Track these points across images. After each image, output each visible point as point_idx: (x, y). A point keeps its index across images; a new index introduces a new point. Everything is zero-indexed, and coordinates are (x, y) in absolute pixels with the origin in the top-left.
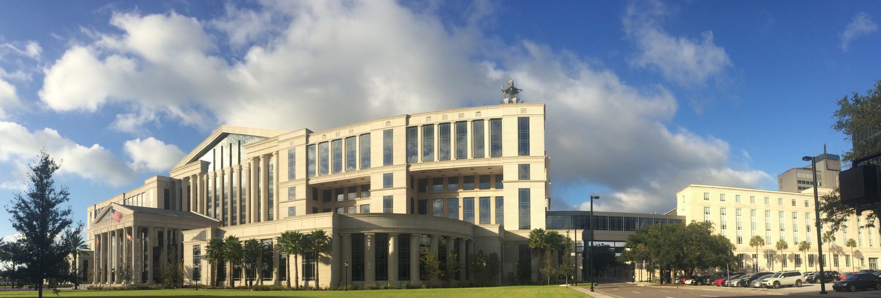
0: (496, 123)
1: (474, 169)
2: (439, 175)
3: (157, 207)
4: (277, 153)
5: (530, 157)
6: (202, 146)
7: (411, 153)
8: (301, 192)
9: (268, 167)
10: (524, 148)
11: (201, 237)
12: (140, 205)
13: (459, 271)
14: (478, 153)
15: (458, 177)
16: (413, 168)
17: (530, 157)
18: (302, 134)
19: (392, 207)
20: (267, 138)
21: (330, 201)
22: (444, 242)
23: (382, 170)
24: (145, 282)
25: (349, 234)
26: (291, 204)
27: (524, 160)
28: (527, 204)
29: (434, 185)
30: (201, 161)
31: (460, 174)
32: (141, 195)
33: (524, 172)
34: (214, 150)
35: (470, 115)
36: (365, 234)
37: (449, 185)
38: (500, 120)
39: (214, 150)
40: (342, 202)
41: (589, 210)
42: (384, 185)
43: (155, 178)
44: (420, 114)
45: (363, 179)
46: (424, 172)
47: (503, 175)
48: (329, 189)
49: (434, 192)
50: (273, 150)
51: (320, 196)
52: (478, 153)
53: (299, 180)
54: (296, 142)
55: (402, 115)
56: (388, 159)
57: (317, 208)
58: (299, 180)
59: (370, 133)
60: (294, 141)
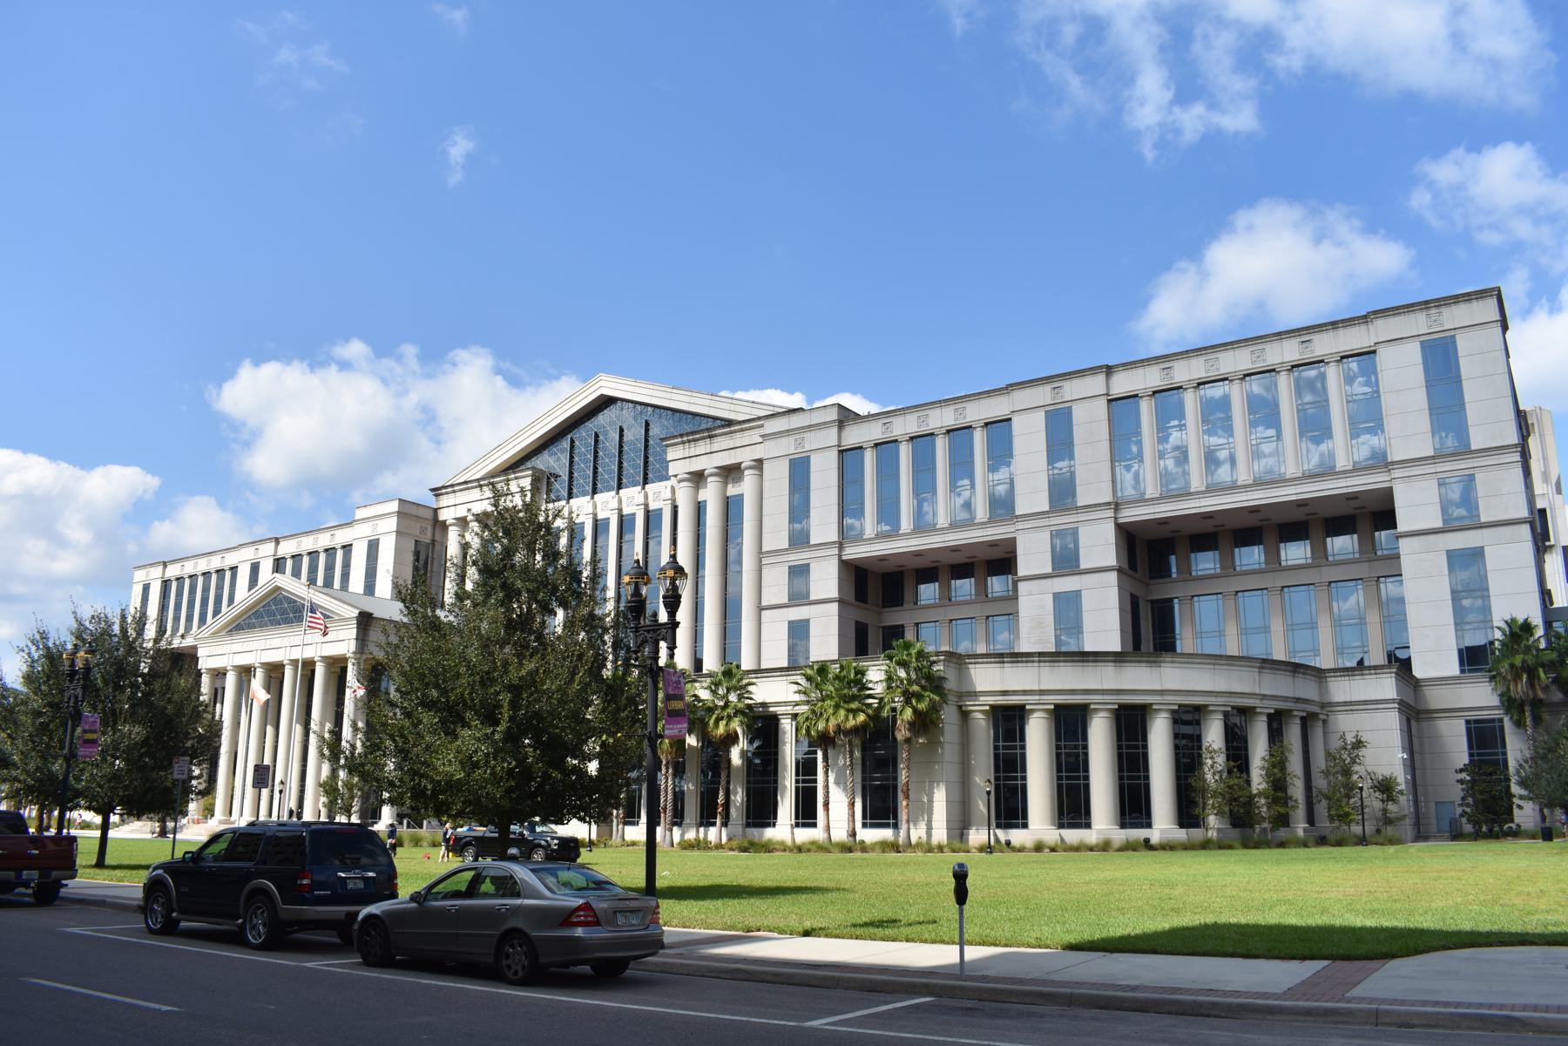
1: (1258, 511)
2: (1208, 527)
3: (1120, 650)
4: (759, 464)
6: (619, 386)
8: (826, 581)
9: (730, 508)
12: (355, 626)
15: (1173, 539)
16: (854, 552)
18: (829, 419)
20: (729, 423)
21: (902, 605)
22: (1237, 720)
24: (74, 779)
25: (987, 708)
26: (797, 613)
29: (1193, 551)
30: (533, 468)
31: (1222, 526)
34: (572, 441)
36: (1028, 707)
37: (953, 582)
39: (572, 441)
40: (665, 624)
43: (394, 506)
45: (993, 544)
46: (1166, 523)
48: (1171, 535)
50: (745, 457)
51: (874, 589)
52: (309, 619)
53: (1088, 508)
54: (812, 441)
57: (866, 625)
58: (1025, 516)
59: (1010, 419)
60: (807, 435)
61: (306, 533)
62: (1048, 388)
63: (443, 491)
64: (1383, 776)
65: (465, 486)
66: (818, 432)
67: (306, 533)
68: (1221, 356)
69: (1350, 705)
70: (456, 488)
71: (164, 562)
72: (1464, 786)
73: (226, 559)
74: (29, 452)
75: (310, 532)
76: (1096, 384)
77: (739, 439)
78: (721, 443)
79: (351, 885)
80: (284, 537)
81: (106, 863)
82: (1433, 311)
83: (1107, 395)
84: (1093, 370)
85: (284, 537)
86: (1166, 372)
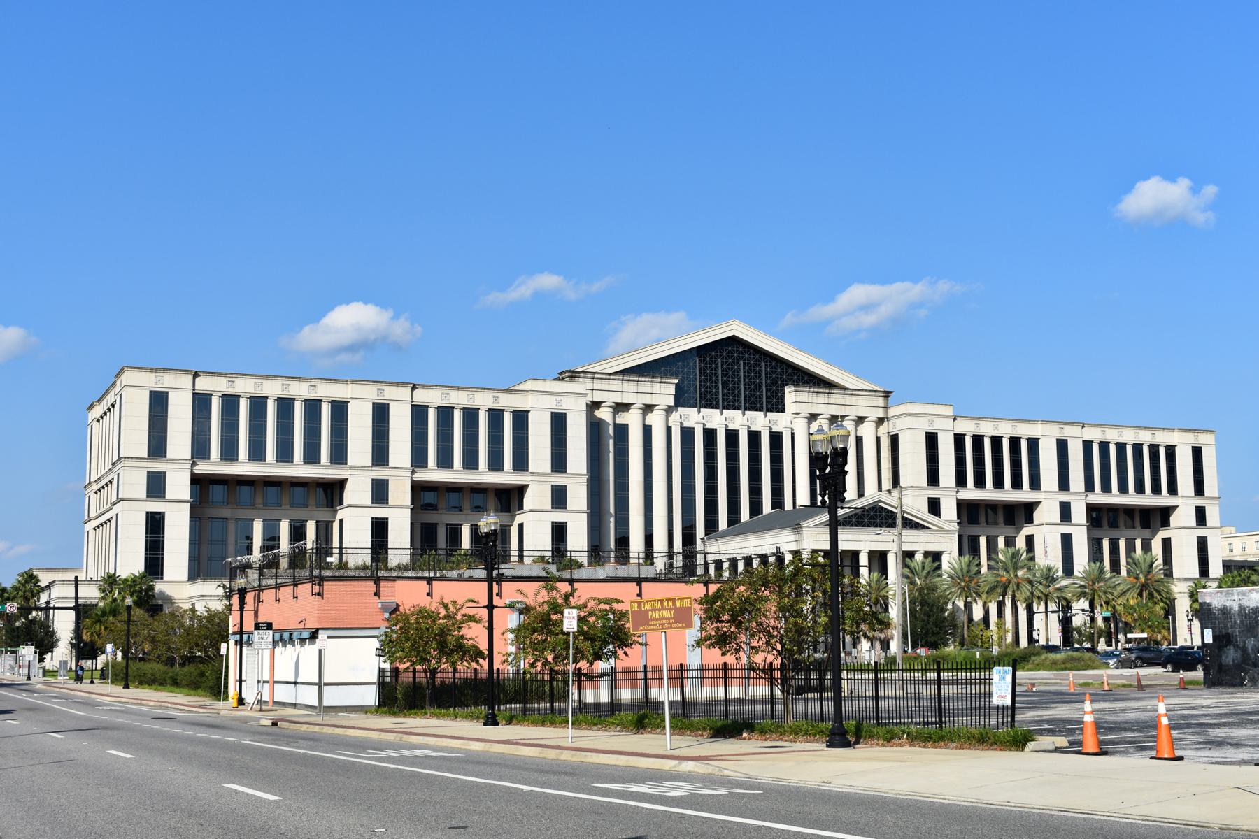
0: (340, 409)
5: (568, 474)
7: (200, 449)
10: (559, 463)
11: (644, 607)
13: (45, 643)
14: (496, 463)
17: (505, 472)
19: (163, 533)
23: (369, 472)
27: (559, 479)
28: (384, 541)
32: (92, 480)
33: (559, 497)
35: (718, 419)
38: (501, 413)
41: (860, 564)
42: (552, 504)
44: (311, 379)
47: (191, 484)
49: (211, 504)
55: (408, 384)
56: (380, 455)
61: (335, 380)
62: (926, 419)
63: (582, 375)
64: (45, 658)
65: (608, 377)
66: (517, 395)
67: (458, 387)
68: (936, 420)
69: (1047, 640)
70: (596, 376)
71: (414, 385)
72: (187, 663)
73: (1106, 433)
74: (1134, 185)
75: (427, 385)
76: (187, 380)
77: (848, 400)
78: (835, 398)
79: (224, 646)
80: (961, 417)
81: (1205, 630)
82: (1196, 434)
83: (888, 433)
84: (405, 384)
85: (961, 417)
86: (380, 391)
